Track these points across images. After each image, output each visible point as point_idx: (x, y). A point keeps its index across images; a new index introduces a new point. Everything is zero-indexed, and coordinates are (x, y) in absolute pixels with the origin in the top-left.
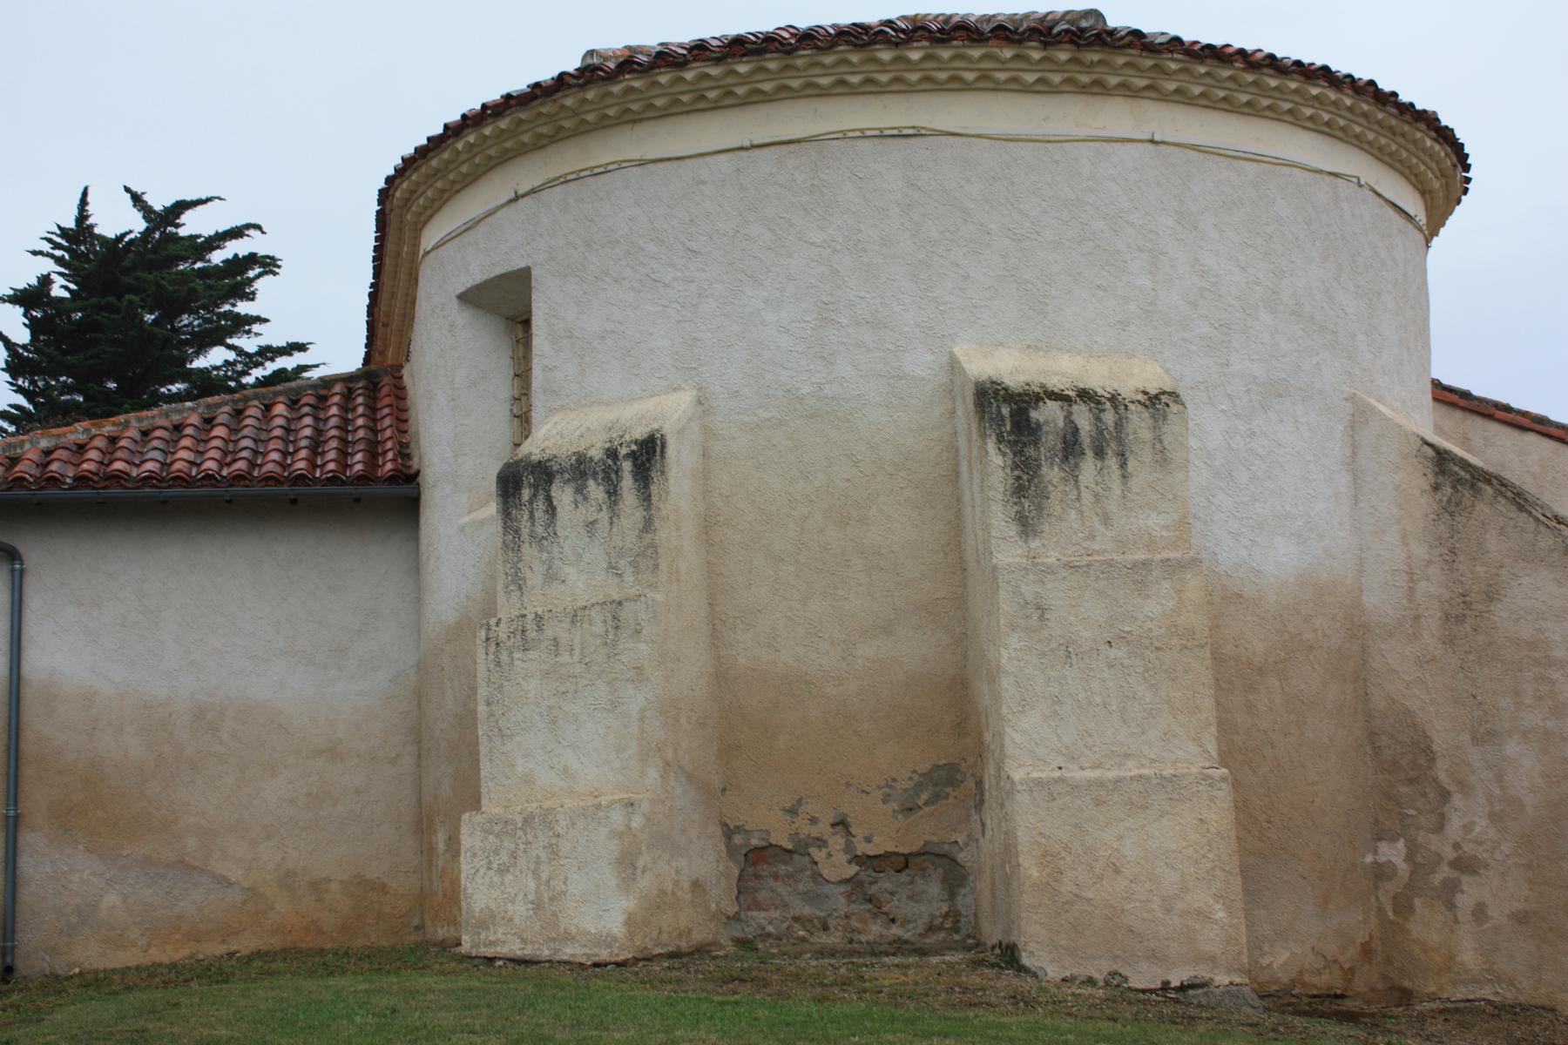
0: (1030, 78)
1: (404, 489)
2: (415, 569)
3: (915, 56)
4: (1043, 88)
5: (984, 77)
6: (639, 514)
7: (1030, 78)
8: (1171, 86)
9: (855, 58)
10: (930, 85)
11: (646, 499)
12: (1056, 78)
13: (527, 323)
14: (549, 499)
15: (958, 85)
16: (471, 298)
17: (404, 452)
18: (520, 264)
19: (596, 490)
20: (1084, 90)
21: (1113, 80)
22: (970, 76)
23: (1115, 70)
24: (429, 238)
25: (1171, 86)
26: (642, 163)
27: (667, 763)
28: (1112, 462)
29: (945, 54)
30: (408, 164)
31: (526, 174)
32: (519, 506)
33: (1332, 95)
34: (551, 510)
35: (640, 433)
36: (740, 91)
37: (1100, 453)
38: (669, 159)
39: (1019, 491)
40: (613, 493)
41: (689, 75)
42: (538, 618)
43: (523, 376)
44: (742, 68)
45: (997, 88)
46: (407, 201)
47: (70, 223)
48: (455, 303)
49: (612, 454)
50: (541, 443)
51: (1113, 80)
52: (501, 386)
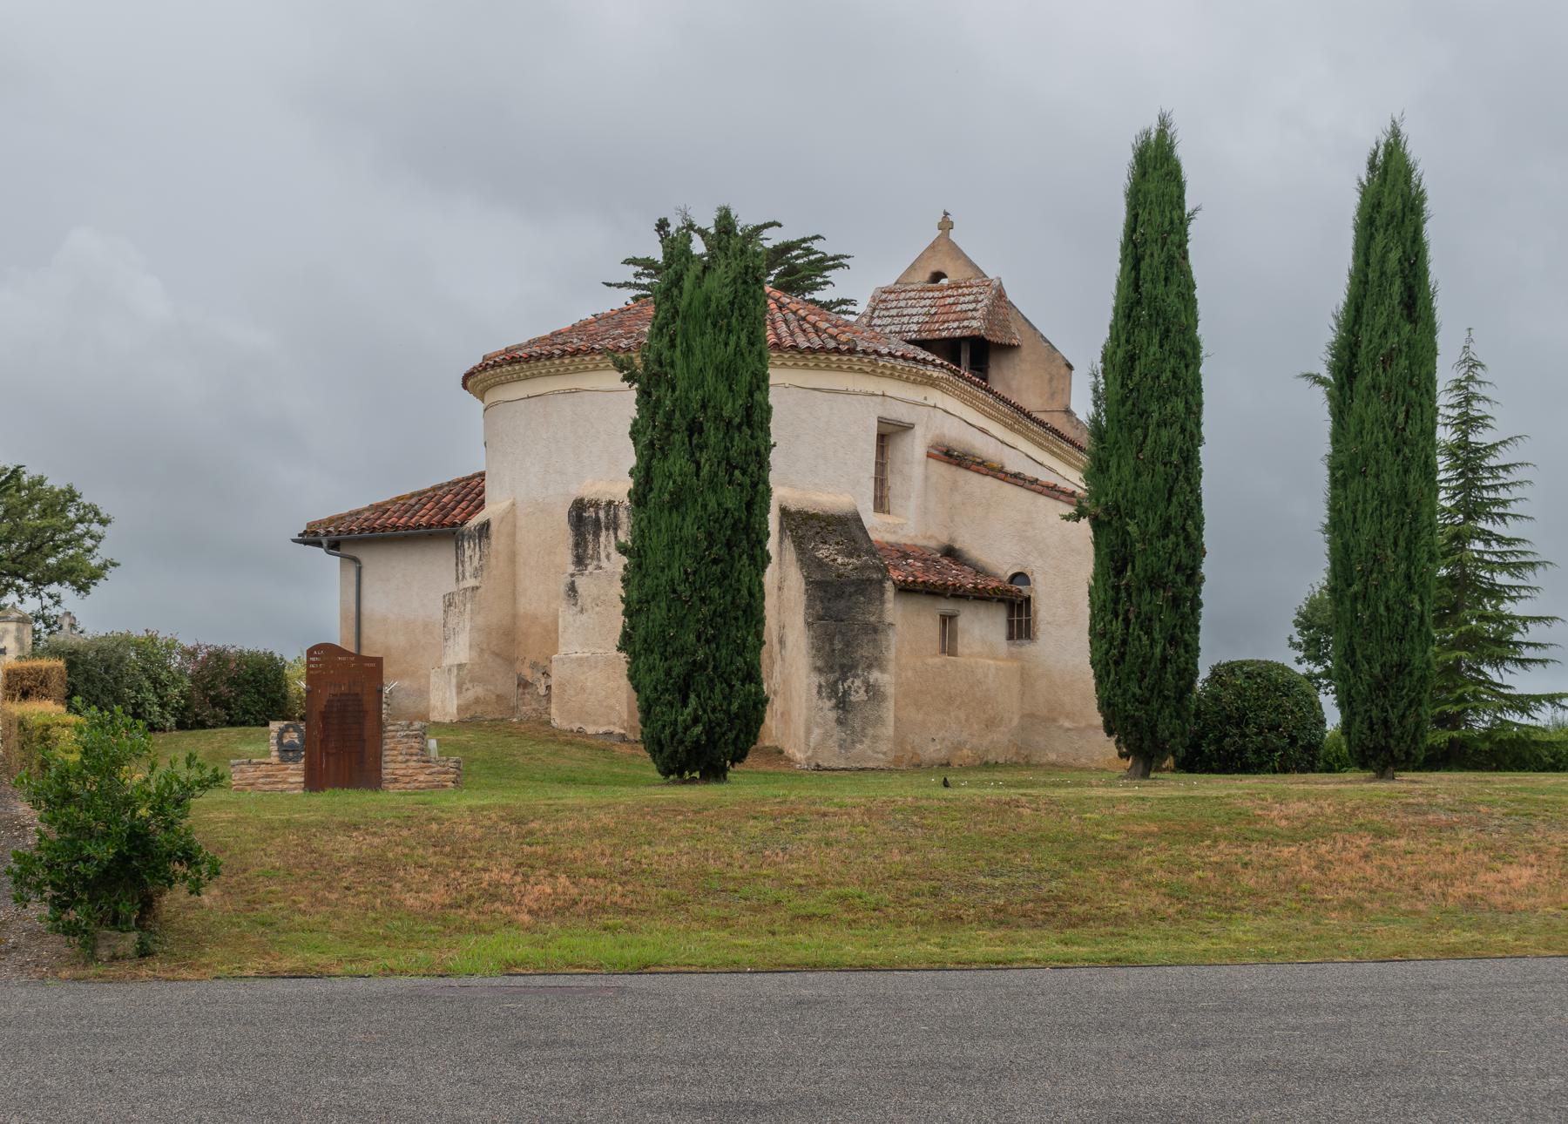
3: (567, 361)
27: (482, 650)
28: (611, 532)
37: (607, 529)
39: (577, 545)
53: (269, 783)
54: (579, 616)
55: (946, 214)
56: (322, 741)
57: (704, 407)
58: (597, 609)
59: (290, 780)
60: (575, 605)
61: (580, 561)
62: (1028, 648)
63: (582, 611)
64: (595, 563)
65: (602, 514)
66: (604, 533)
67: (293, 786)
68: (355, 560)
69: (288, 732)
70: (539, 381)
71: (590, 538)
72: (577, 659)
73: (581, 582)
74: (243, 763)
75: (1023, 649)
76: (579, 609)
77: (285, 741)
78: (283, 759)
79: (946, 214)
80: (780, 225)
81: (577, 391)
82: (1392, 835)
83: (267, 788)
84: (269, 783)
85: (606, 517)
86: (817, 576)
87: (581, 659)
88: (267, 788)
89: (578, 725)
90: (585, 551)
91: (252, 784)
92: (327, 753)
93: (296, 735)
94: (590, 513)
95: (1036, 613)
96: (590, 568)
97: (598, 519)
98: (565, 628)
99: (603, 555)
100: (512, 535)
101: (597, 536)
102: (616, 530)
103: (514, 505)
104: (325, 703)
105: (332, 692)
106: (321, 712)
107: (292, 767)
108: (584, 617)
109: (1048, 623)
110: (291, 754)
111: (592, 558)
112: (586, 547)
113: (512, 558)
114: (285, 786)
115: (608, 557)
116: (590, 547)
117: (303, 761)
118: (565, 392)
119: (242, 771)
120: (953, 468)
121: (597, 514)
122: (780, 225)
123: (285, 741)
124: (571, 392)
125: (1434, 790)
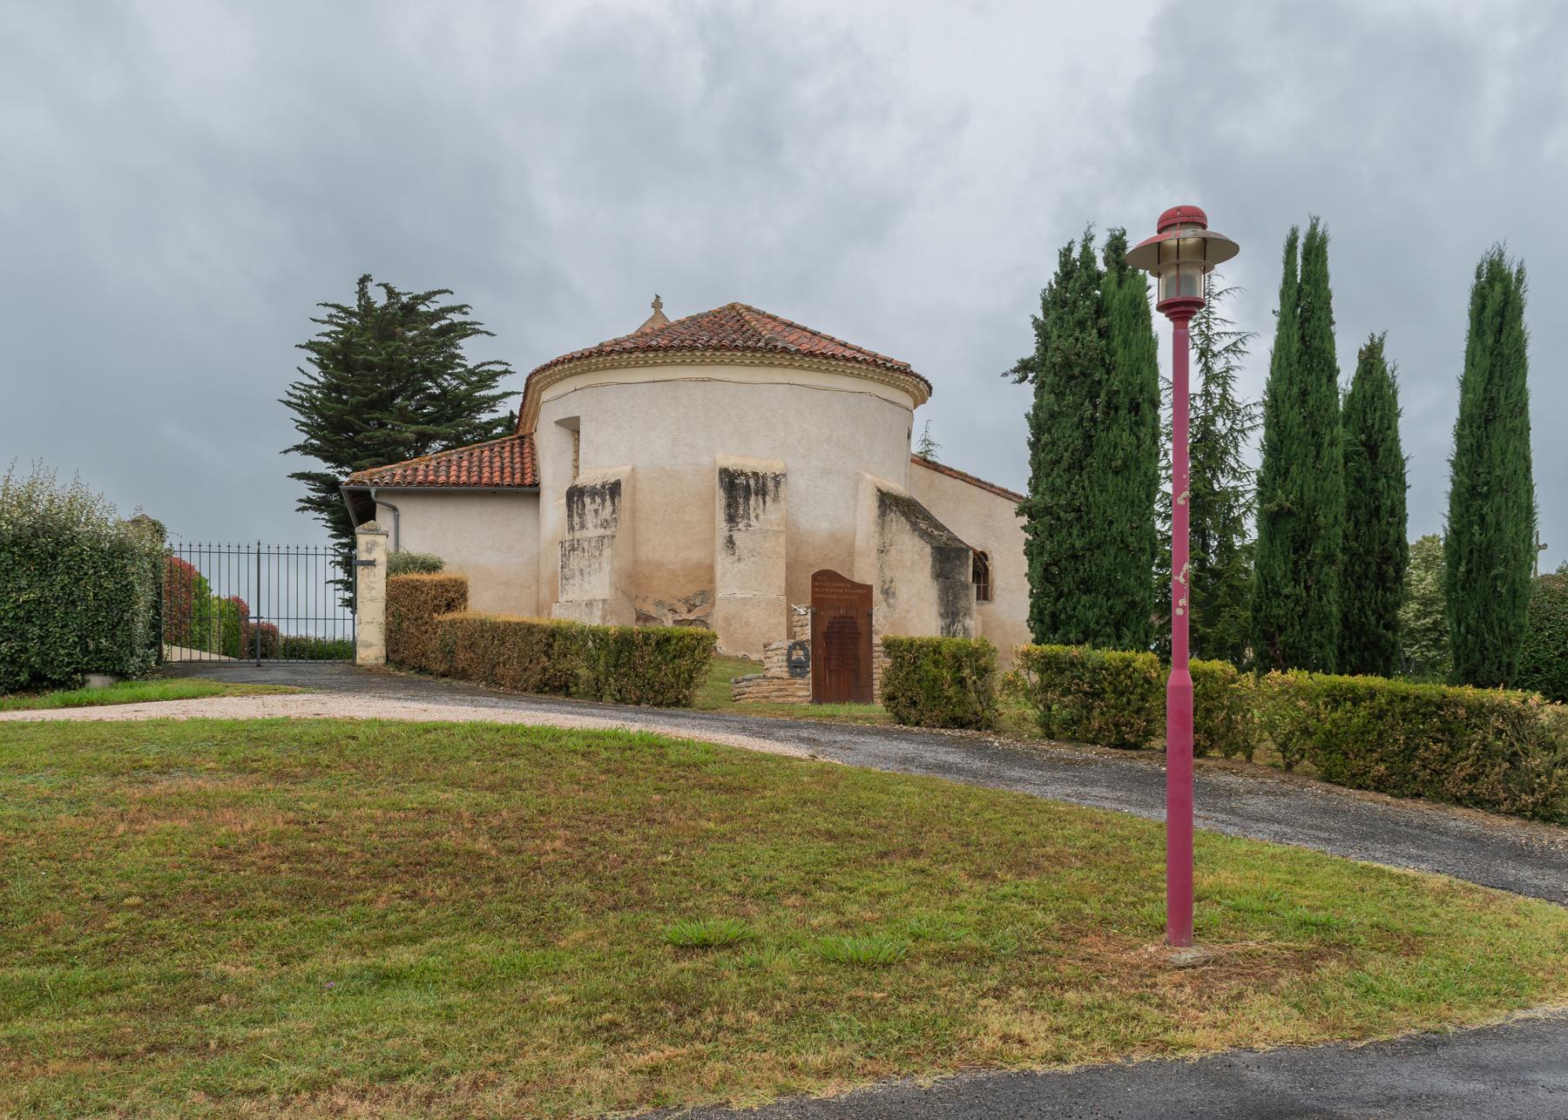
0: (748, 362)
1: (534, 489)
2: (538, 518)
3: (708, 354)
4: (752, 364)
5: (732, 361)
6: (1092, 245)
7: (748, 362)
8: (797, 364)
9: (688, 354)
10: (713, 363)
11: (613, 503)
12: (756, 362)
13: (579, 432)
14: (583, 501)
15: (722, 363)
16: (559, 423)
17: (534, 474)
18: (576, 415)
19: (598, 500)
20: (767, 365)
21: (776, 363)
22: (727, 361)
23: (777, 360)
24: (546, 395)
25: (797, 364)
26: (618, 384)
27: (617, 588)
28: (760, 497)
29: (718, 354)
30: (537, 372)
31: (579, 381)
32: (573, 503)
33: (857, 365)
34: (584, 505)
35: (612, 480)
36: (651, 362)
37: (757, 494)
38: (576, 460)
39: (729, 506)
40: (604, 501)
41: (633, 356)
42: (578, 540)
43: (577, 452)
44: (651, 355)
45: (737, 364)
46: (537, 382)
47: (353, 303)
48: (553, 425)
49: (603, 487)
50: (583, 480)
51: (776, 363)
52: (570, 456)
53: (782, 697)
54: (737, 564)
55: (657, 297)
56: (825, 659)
57: (1141, 391)
58: (753, 559)
59: (800, 694)
60: (734, 554)
61: (731, 519)
62: (987, 607)
63: (739, 560)
64: (746, 521)
65: (752, 482)
66: (753, 498)
67: (801, 699)
68: (395, 509)
69: (795, 649)
70: (670, 368)
71: (741, 501)
72: (742, 599)
73: (737, 536)
74: (759, 678)
75: (983, 607)
76: (737, 558)
77: (794, 658)
78: (793, 675)
79: (657, 297)
80: (452, 293)
81: (709, 380)
82: (166, 770)
83: (780, 700)
84: (782, 697)
85: (756, 485)
86: (935, 544)
87: (745, 599)
88: (780, 700)
89: (743, 653)
90: (736, 511)
91: (767, 697)
92: (830, 670)
93: (802, 653)
94: (742, 480)
95: (993, 581)
96: (740, 526)
97: (748, 486)
98: (724, 574)
99: (752, 516)
100: (633, 494)
101: (747, 499)
102: (764, 495)
103: (633, 469)
104: (826, 624)
105: (833, 614)
106: (824, 633)
107: (799, 681)
108: (741, 565)
109: (1004, 589)
110: (798, 670)
111: (743, 517)
112: (738, 508)
113: (633, 512)
114: (795, 699)
115: (757, 517)
116: (741, 508)
117: (810, 675)
118: (697, 380)
119: (758, 685)
120: (931, 471)
121: (747, 482)
122: (452, 293)
123: (794, 658)
124: (703, 380)
125: (829, 716)
